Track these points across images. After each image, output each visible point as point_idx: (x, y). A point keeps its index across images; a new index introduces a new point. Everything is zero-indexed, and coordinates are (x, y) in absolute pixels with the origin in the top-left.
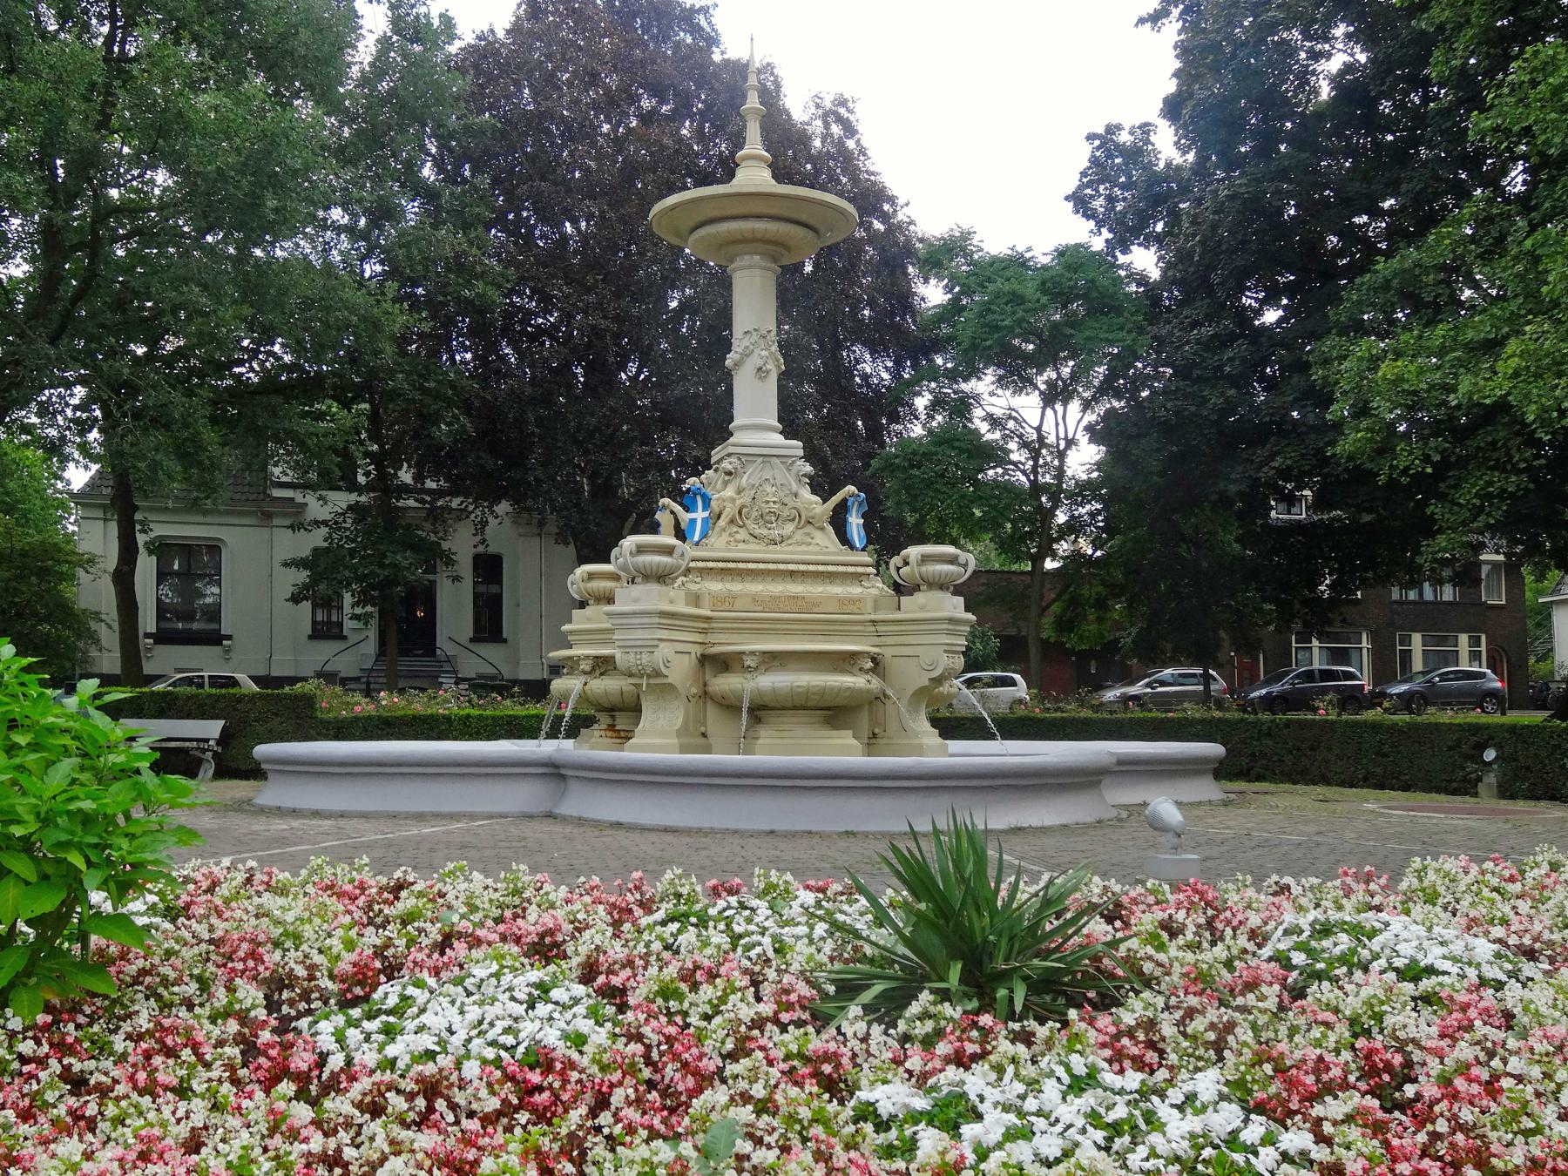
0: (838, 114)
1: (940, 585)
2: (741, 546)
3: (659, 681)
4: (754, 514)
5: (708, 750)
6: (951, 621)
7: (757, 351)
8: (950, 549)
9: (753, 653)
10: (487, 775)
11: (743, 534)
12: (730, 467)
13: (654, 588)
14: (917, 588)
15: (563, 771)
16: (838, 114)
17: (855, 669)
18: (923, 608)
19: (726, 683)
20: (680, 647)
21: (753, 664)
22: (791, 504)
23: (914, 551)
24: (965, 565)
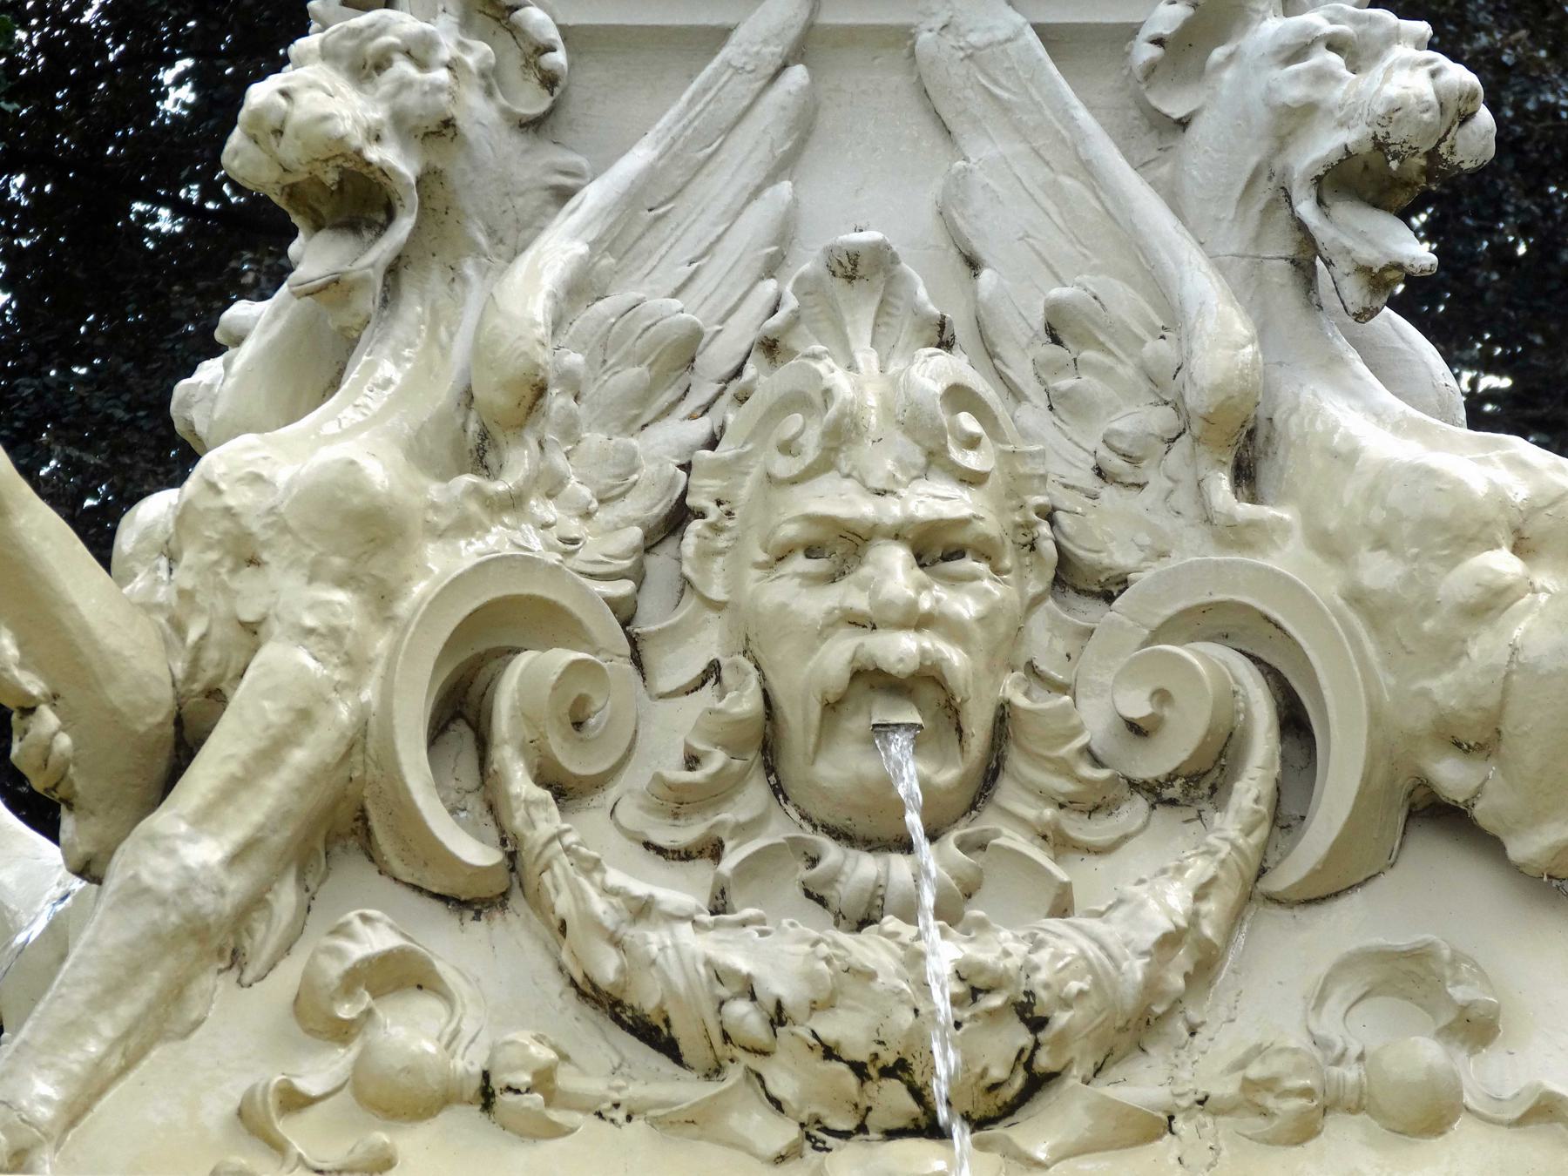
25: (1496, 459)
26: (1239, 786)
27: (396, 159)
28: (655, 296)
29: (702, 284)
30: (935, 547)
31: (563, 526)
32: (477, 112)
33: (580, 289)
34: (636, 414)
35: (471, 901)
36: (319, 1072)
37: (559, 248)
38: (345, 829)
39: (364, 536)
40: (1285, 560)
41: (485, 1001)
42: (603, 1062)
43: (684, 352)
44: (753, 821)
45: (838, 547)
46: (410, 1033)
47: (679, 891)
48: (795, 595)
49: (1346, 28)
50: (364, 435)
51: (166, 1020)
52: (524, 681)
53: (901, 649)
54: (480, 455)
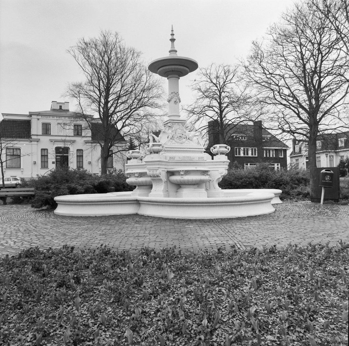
0: (30, 112)
1: (222, 153)
2: (174, 144)
3: (158, 178)
4: (176, 137)
5: (169, 197)
6: (224, 162)
7: (175, 97)
8: (225, 145)
9: (183, 171)
10: (225, 205)
11: (174, 142)
12: (170, 125)
13: (156, 155)
14: (217, 154)
15: (140, 202)
16: (30, 112)
17: (206, 174)
18: (219, 159)
19: (174, 178)
20: (164, 169)
21: (183, 174)
22: (184, 134)
23: (218, 146)
24: (228, 149)
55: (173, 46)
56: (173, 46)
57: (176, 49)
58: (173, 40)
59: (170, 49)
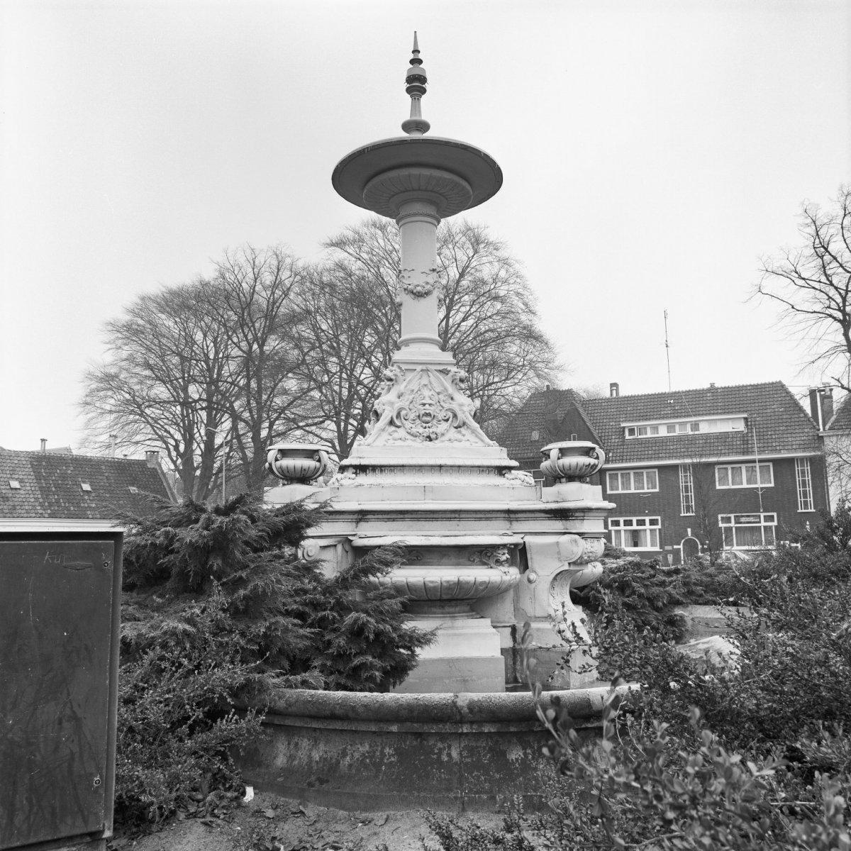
25: (122, 625)
26: (89, 455)
27: (393, 377)
28: (411, 387)
29: (415, 386)
30: (430, 405)
31: (404, 403)
32: (399, 374)
33: (406, 386)
34: (409, 395)
35: (398, 427)
36: (390, 437)
37: (405, 383)
38: (391, 423)
39: (392, 404)
40: (454, 406)
41: (401, 433)
42: (409, 437)
43: (413, 391)
44: (418, 422)
45: (424, 405)
46: (396, 435)
47: (413, 426)
48: (421, 407)
49: (367, 558)
50: (265, 306)
51: (379, 435)
52: (403, 413)
53: (427, 412)
54: (399, 397)
55: (415, 108)
56: (415, 108)
57: (425, 117)
58: (416, 84)
59: (406, 117)
